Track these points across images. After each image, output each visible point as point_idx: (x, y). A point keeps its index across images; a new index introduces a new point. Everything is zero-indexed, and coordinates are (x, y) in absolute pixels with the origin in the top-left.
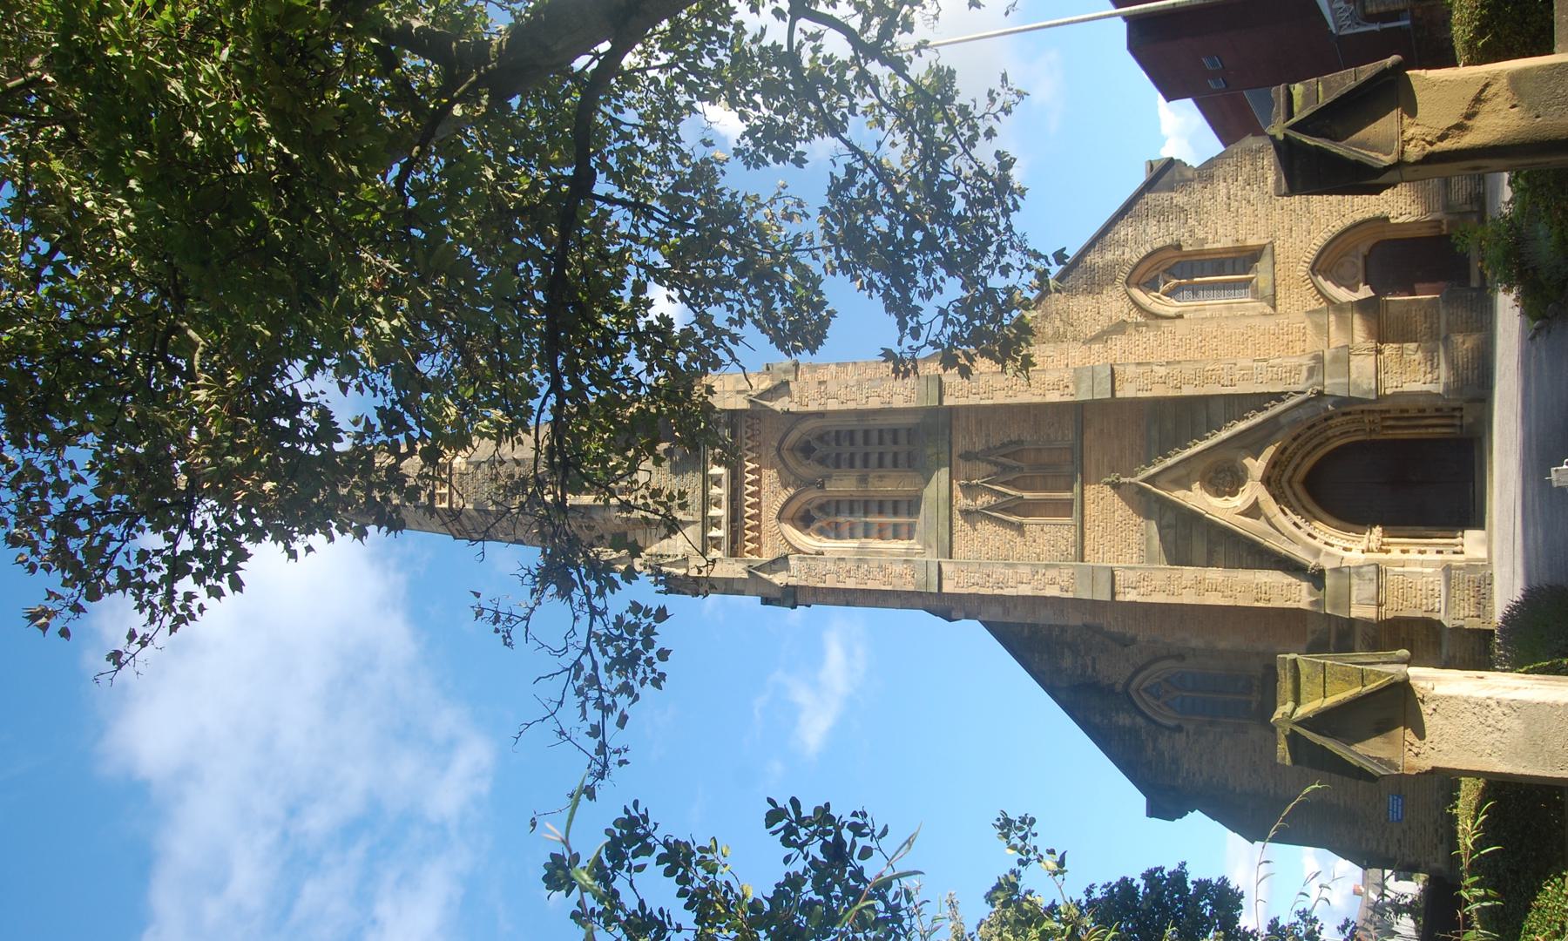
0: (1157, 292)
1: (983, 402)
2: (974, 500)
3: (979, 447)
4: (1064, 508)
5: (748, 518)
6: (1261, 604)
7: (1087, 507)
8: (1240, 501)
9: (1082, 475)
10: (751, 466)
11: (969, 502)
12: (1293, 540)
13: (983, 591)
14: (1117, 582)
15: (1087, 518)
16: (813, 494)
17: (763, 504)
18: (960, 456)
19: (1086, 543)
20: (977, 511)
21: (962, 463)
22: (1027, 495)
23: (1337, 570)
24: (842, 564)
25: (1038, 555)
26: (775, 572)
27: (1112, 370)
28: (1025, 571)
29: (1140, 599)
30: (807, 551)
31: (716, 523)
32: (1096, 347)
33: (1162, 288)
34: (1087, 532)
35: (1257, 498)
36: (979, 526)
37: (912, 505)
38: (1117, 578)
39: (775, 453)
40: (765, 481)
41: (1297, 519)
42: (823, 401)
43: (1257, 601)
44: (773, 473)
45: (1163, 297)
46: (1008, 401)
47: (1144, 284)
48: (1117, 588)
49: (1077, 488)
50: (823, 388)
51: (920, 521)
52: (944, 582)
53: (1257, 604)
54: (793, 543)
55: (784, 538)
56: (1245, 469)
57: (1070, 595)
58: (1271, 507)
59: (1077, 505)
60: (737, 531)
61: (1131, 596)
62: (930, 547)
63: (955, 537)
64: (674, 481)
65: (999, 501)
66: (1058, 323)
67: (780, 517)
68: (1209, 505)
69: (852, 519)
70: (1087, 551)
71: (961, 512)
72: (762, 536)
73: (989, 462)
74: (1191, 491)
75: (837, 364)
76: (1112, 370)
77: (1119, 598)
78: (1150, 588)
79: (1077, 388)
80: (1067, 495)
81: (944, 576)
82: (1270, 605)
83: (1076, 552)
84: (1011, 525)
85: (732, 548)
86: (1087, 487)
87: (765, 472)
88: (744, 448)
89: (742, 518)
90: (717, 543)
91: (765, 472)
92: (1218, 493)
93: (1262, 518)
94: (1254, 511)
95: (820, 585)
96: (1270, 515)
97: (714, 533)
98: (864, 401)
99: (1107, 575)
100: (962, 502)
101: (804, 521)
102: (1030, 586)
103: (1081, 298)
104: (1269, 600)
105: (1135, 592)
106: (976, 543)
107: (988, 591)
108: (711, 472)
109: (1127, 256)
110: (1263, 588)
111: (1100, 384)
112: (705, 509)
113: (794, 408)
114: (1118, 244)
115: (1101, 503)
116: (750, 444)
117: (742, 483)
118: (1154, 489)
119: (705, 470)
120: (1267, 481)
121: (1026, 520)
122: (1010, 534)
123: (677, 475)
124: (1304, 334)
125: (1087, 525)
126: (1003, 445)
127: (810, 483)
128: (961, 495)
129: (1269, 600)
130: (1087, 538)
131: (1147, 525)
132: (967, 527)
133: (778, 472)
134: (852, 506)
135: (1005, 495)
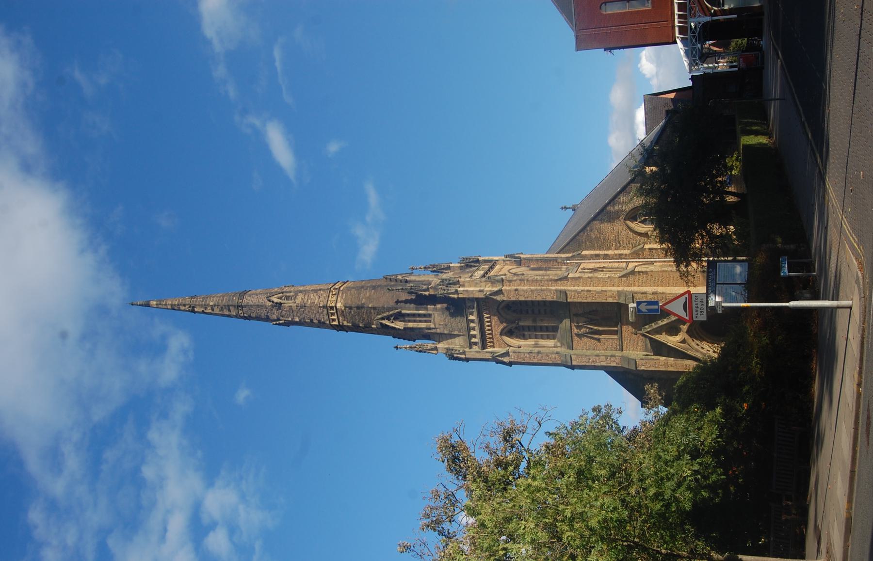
0: (637, 221)
1: (583, 301)
2: (580, 330)
3: (580, 312)
4: (615, 333)
5: (488, 334)
7: (623, 333)
8: (678, 338)
10: (486, 316)
11: (578, 330)
12: (697, 351)
13: (587, 364)
14: (637, 364)
15: (623, 337)
16: (514, 325)
17: (493, 329)
18: (574, 315)
19: (624, 344)
20: (582, 334)
21: (574, 317)
22: (600, 328)
24: (531, 354)
25: (606, 349)
26: (504, 357)
27: (633, 295)
28: (603, 358)
29: (645, 369)
31: (474, 336)
32: (624, 279)
33: (638, 220)
34: (624, 341)
35: (684, 339)
36: (583, 339)
37: (555, 329)
40: (493, 321)
41: (698, 342)
42: (517, 297)
44: (496, 318)
45: (639, 224)
46: (593, 301)
47: (631, 218)
49: (619, 326)
50: (517, 292)
51: (559, 334)
52: (573, 361)
54: (506, 342)
55: (503, 341)
56: (680, 329)
57: (620, 365)
59: (620, 332)
61: (643, 368)
62: (564, 345)
63: (574, 343)
64: (452, 320)
65: (590, 330)
66: (596, 233)
67: (501, 334)
68: (668, 340)
69: (529, 333)
70: (624, 347)
71: (576, 334)
73: (585, 318)
75: (520, 280)
76: (633, 295)
77: (639, 369)
79: (619, 299)
81: (572, 359)
84: (595, 339)
86: (623, 326)
87: (492, 317)
88: (483, 309)
90: (476, 344)
91: (492, 317)
92: (671, 335)
94: (684, 341)
96: (689, 343)
97: (474, 340)
98: (535, 298)
99: (634, 361)
100: (575, 331)
101: (510, 333)
102: (605, 363)
103: (606, 224)
108: (469, 318)
109: (624, 208)
111: (628, 299)
112: (469, 332)
113: (505, 299)
114: (620, 203)
116: (485, 308)
119: (467, 318)
120: (688, 332)
121: (600, 337)
122: (595, 342)
123: (453, 317)
124: (699, 279)
126: (590, 312)
127: (513, 322)
128: (575, 328)
130: (624, 343)
132: (578, 339)
133: (498, 318)
134: (529, 328)
135: (592, 329)
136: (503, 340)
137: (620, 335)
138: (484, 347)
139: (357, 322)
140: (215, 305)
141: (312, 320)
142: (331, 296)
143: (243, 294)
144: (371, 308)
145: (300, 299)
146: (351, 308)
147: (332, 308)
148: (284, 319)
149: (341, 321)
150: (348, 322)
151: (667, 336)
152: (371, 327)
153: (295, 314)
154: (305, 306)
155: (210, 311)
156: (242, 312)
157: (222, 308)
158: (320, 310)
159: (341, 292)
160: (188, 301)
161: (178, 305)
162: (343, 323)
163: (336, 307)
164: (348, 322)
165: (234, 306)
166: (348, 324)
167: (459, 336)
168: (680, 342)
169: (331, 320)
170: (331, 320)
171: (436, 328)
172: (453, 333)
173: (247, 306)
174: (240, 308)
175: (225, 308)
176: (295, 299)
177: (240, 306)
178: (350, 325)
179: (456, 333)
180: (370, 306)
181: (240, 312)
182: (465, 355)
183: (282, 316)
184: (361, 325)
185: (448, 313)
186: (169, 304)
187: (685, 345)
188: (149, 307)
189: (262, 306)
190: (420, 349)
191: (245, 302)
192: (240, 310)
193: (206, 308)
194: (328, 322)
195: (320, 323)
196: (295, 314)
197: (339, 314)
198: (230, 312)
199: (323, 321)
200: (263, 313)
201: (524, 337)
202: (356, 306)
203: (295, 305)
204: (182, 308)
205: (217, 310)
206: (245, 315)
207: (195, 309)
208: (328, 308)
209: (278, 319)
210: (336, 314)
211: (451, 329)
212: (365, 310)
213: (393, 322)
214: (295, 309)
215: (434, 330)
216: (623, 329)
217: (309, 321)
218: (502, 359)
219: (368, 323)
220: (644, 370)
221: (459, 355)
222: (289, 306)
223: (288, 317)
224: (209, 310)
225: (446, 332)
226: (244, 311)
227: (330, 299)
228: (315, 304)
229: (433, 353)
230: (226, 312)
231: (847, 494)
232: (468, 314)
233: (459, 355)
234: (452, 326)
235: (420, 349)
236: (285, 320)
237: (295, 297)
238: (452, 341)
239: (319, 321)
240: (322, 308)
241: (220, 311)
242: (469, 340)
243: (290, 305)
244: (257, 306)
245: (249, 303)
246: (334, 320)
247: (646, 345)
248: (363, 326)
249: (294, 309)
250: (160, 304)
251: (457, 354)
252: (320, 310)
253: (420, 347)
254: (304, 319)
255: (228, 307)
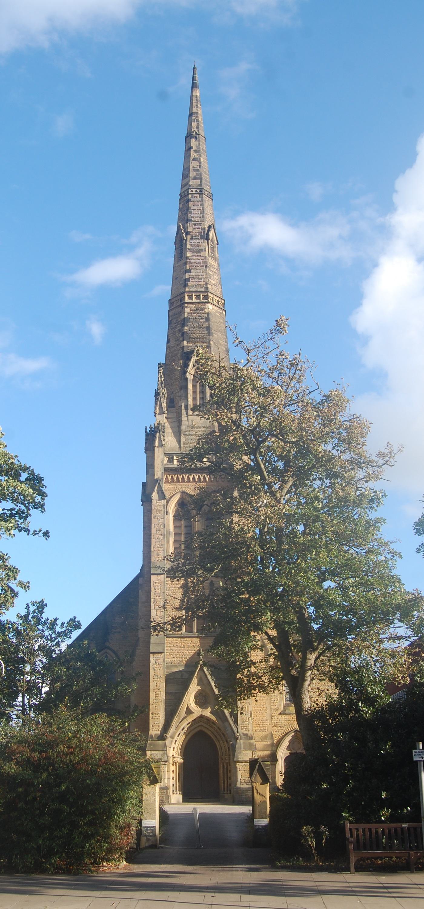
6: (150, 715)
7: (190, 639)
8: (193, 706)
9: (204, 637)
12: (177, 728)
13: (152, 594)
14: (158, 655)
15: (185, 639)
17: (189, 484)
19: (174, 639)
23: (165, 745)
24: (162, 527)
26: (158, 493)
29: (151, 664)
30: (168, 506)
34: (179, 639)
35: (194, 713)
38: (160, 655)
39: (213, 489)
41: (186, 729)
43: (152, 713)
48: (156, 655)
52: (156, 576)
53: (150, 713)
54: (173, 498)
55: (174, 495)
56: (206, 708)
58: (190, 719)
60: (177, 471)
61: (152, 661)
72: (174, 483)
74: (197, 685)
77: (151, 656)
78: (156, 669)
80: (195, 630)
81: (158, 576)
82: (150, 718)
83: (170, 634)
85: (169, 469)
86: (198, 639)
89: (183, 473)
92: (196, 697)
93: (186, 715)
94: (189, 712)
95: (153, 515)
96: (187, 718)
104: (152, 718)
105: (154, 662)
106: (174, 589)
107: (152, 597)
110: (157, 716)
115: (192, 645)
117: (199, 473)
118: (197, 670)
120: (201, 717)
124: (263, 731)
125: (182, 639)
129: (152, 718)
130: (176, 639)
131: (182, 665)
136: (175, 494)
137: (186, 636)
138: (167, 470)
139: (190, 324)
140: (200, 163)
141: (189, 271)
142: (217, 299)
143: (211, 196)
144: (209, 343)
145: (213, 263)
146: (207, 319)
147: (206, 297)
148: (188, 240)
149: (190, 305)
150: (188, 313)
151: (195, 692)
152: (183, 340)
153: (195, 254)
154: (206, 267)
155: (192, 156)
156: (194, 192)
157: (198, 170)
158: (202, 283)
159: (221, 312)
160: (202, 133)
161: (197, 121)
162: (187, 307)
163: (208, 302)
164: (188, 313)
165: (201, 185)
166: (186, 314)
167: (179, 442)
168: (188, 707)
169: (190, 294)
170: (190, 294)
171: (188, 416)
172: (182, 435)
173: (202, 199)
174: (198, 191)
175: (197, 174)
176: (211, 257)
177: (201, 191)
178: (186, 316)
179: (183, 439)
180: (211, 342)
181: (194, 190)
182: (157, 447)
183: (192, 238)
184: (186, 328)
185: (207, 432)
186: (197, 110)
187: (183, 714)
188: (193, 88)
189: (203, 217)
190: (161, 393)
191: (206, 198)
192: (196, 191)
193: (196, 152)
194: (187, 290)
195: (185, 281)
196: (195, 254)
197: (199, 304)
198: (193, 179)
199: (189, 284)
200: (194, 216)
201: (176, 517)
202: (211, 326)
203: (207, 256)
204: (194, 125)
205: (194, 164)
206: (190, 196)
207: (194, 139)
208: (206, 294)
209: (187, 233)
210: (198, 301)
211: (187, 433)
212: (205, 335)
213: (194, 366)
214: (202, 254)
215: (185, 413)
216: (195, 639)
217: (188, 268)
218: (156, 491)
219: (189, 338)
220: (150, 662)
221: (158, 438)
222: (205, 249)
223: (191, 245)
224: (193, 154)
225: (183, 427)
226: (195, 195)
227: (215, 297)
228: (210, 280)
229: (155, 408)
230: (192, 174)
231: (213, 894)
232: (210, 456)
233: (158, 438)
234: (192, 435)
235: (161, 393)
236: (186, 240)
237: (213, 258)
238: (170, 434)
239: (188, 280)
240: (205, 285)
241: (193, 167)
242: (175, 454)
243: (207, 250)
244: (203, 211)
245: (205, 202)
246: (190, 297)
247: (176, 666)
248: (185, 331)
249: (202, 253)
250: (197, 100)
251: (160, 438)
252: (202, 283)
253: (163, 394)
254: (190, 263)
255: (199, 177)
